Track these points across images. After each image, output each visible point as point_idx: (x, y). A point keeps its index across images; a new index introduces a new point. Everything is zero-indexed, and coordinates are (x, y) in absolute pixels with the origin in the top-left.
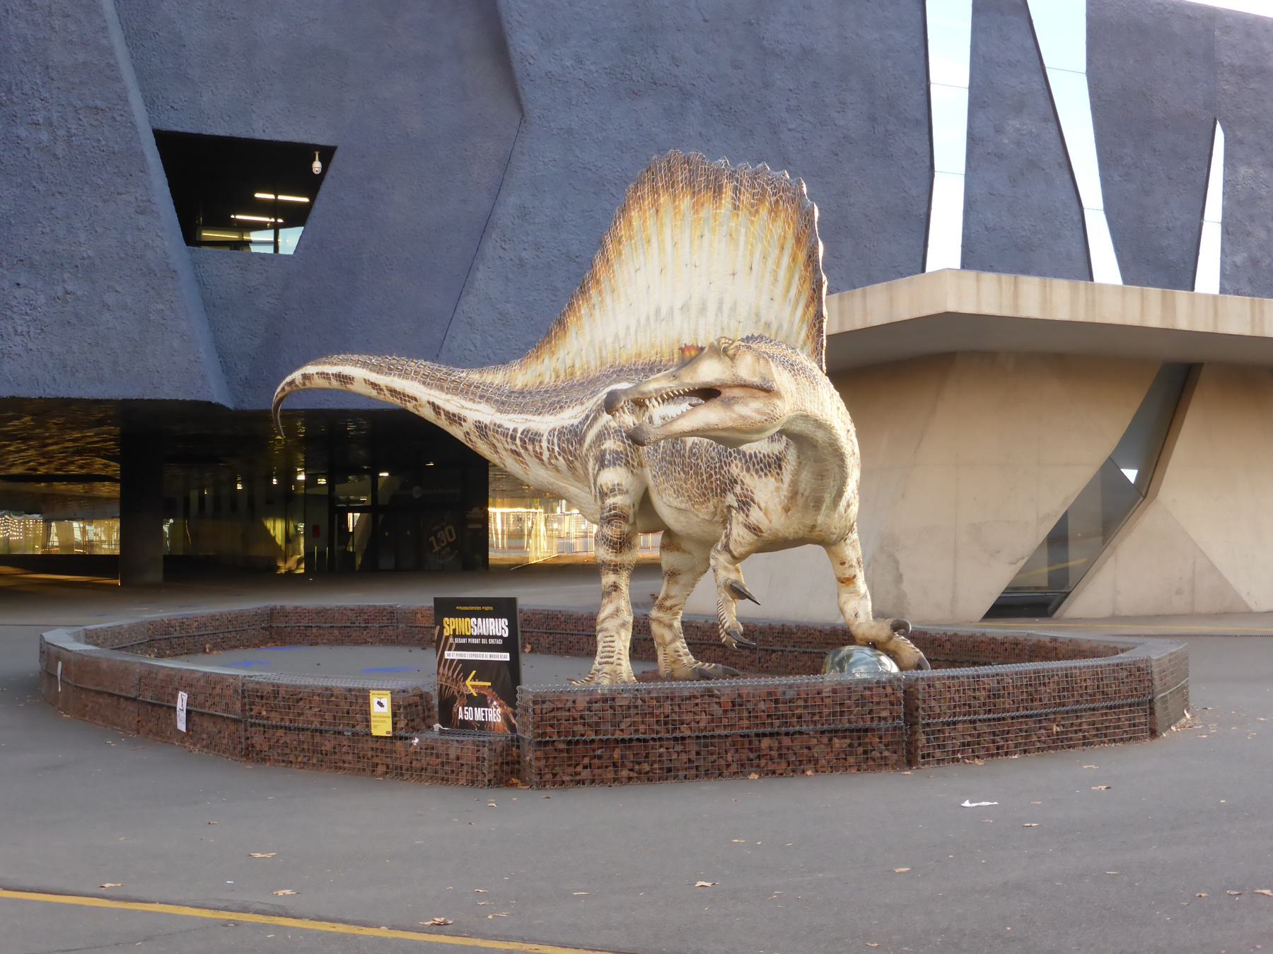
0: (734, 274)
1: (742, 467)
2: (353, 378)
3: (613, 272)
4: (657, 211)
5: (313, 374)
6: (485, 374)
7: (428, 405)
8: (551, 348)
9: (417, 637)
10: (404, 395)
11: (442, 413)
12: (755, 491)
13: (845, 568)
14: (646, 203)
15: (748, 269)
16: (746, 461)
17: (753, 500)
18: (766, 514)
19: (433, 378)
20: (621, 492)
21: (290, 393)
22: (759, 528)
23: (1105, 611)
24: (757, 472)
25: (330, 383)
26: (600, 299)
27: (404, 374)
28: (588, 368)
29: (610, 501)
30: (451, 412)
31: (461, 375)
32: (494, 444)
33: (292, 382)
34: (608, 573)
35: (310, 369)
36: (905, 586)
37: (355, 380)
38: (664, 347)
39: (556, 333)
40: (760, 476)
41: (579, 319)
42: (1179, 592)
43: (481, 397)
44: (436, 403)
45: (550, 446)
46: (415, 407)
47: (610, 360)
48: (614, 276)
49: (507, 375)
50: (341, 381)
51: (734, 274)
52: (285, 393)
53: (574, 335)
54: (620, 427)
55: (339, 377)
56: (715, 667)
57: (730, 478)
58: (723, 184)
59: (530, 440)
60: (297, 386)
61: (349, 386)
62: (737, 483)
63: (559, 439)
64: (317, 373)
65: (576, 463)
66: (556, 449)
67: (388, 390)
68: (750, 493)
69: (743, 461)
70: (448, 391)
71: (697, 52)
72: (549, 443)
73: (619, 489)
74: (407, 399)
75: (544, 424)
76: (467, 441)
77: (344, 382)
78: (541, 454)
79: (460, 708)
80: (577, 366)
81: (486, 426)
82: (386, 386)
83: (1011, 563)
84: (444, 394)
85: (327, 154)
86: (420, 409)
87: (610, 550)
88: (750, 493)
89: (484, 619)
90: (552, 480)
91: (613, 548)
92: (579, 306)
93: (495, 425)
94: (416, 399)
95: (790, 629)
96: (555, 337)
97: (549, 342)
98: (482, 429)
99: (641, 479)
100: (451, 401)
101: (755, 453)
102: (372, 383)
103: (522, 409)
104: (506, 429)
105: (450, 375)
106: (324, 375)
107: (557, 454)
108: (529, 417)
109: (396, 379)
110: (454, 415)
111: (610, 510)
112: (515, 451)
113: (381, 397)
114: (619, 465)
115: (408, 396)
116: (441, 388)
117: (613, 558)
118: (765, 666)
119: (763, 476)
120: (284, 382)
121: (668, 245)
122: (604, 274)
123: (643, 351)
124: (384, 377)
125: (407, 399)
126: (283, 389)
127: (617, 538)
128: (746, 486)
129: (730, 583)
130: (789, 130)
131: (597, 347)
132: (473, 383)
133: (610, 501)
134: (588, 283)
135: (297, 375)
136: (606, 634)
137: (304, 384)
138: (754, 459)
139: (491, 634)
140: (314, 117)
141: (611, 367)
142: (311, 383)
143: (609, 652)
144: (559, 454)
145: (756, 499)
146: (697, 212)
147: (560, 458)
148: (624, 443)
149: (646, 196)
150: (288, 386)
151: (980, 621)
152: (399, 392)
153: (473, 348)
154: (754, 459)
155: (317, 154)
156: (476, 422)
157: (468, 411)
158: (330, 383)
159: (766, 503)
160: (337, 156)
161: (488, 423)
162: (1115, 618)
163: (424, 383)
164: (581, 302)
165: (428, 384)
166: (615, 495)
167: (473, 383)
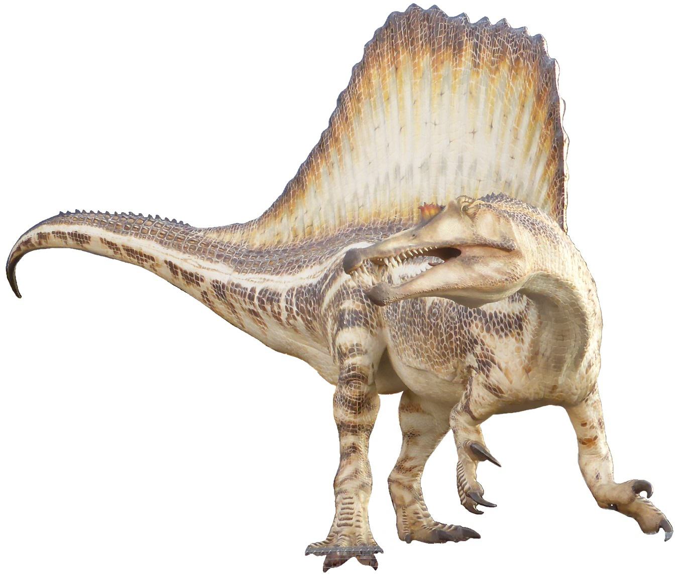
2: (90, 237)
4: (397, 69)
5: (49, 234)
7: (165, 265)
8: (289, 207)
10: (141, 254)
12: (494, 351)
14: (386, 60)
15: (488, 127)
16: (487, 322)
17: (493, 361)
18: (506, 375)
22: (499, 389)
24: (497, 332)
29: (349, 361)
30: (188, 271)
32: (231, 304)
37: (91, 239)
38: (403, 206)
39: (294, 192)
40: (501, 337)
41: (318, 178)
43: (219, 256)
45: (289, 306)
47: (349, 219)
48: (353, 134)
49: (245, 235)
53: (313, 194)
58: (462, 42)
63: (297, 299)
64: (53, 233)
66: (295, 309)
67: (124, 249)
68: (490, 353)
69: (484, 321)
70: (186, 250)
72: (287, 303)
74: (144, 258)
77: (80, 241)
78: (279, 314)
81: (224, 286)
82: (123, 246)
84: (181, 253)
87: (349, 411)
88: (490, 353)
91: (352, 409)
93: (233, 284)
94: (153, 259)
96: (293, 195)
100: (189, 261)
103: (260, 269)
104: (244, 288)
107: (295, 314)
108: (268, 276)
109: (133, 238)
110: (191, 274)
114: (358, 324)
116: (179, 248)
117: (352, 419)
121: (408, 102)
125: (144, 258)
127: (356, 399)
131: (336, 206)
132: (211, 243)
138: (494, 319)
141: (350, 226)
142: (47, 242)
144: (298, 314)
145: (497, 359)
146: (436, 69)
147: (299, 318)
149: (385, 53)
152: (136, 252)
156: (213, 281)
159: (507, 363)
161: (226, 283)
163: (161, 242)
164: (319, 161)
165: (166, 244)
166: (354, 356)
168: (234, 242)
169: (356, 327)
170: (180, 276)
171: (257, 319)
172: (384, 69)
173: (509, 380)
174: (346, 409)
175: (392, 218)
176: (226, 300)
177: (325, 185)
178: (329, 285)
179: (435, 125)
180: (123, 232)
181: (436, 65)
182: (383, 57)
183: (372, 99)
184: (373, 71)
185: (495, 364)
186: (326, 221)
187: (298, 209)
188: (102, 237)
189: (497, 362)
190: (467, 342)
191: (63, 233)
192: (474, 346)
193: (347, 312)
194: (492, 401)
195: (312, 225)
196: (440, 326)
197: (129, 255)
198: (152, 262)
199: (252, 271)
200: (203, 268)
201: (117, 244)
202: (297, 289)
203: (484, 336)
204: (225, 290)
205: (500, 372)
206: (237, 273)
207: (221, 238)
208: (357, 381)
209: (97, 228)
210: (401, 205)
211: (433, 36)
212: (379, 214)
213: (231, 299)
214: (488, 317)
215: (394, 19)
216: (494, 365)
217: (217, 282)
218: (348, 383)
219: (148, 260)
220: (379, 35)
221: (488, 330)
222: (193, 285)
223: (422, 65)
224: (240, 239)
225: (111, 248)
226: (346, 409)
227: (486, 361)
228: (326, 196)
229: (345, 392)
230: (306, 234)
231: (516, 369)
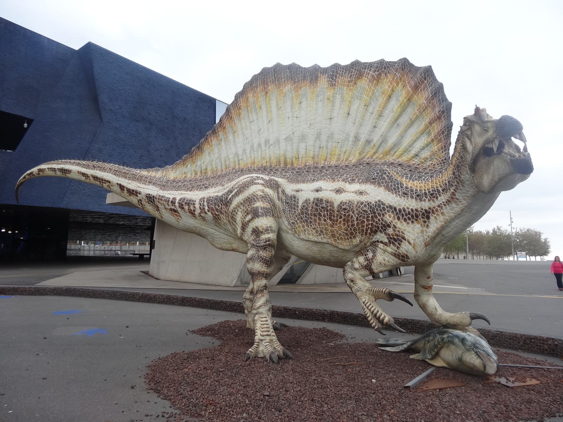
0: (331, 119)
1: (394, 217)
2: (71, 171)
3: (235, 123)
4: (267, 93)
5: (45, 169)
6: (151, 172)
7: (117, 185)
8: (192, 160)
9: (72, 293)
10: (102, 180)
11: (125, 189)
12: (405, 232)
13: (430, 280)
14: (259, 89)
15: (346, 115)
16: (397, 214)
17: (404, 238)
18: (413, 247)
19: (120, 172)
20: (272, 231)
21: (25, 181)
22: (407, 256)
23: (312, 282)
24: (405, 220)
25: (56, 173)
26: (225, 136)
27: (104, 170)
28: (216, 170)
29: (264, 237)
30: (131, 189)
31: (137, 172)
32: (157, 206)
33: (32, 173)
34: (262, 279)
35: (43, 166)
37: (72, 172)
38: (272, 158)
39: (196, 153)
40: (408, 223)
41: (211, 146)
42: (333, 276)
43: (150, 182)
44: (122, 184)
45: (202, 207)
46: (109, 186)
47: (232, 165)
48: (235, 125)
49: (164, 173)
50: (62, 172)
51: (331, 119)
52: (26, 179)
53: (207, 154)
54: (265, 195)
55: (62, 170)
57: (384, 223)
58: (318, 76)
59: (186, 203)
60: (34, 175)
61: (68, 175)
62: (390, 227)
63: (208, 203)
64: (48, 168)
65: (221, 216)
66: (206, 208)
67: (92, 177)
68: (401, 233)
69: (395, 213)
70: (129, 178)
71: (156, 113)
72: (200, 205)
73: (271, 230)
74: (104, 182)
75: (196, 196)
76: (139, 204)
77: (65, 173)
78: (194, 211)
80: (209, 169)
81: (153, 197)
82: (92, 175)
84: (127, 180)
85: (30, 122)
86: (111, 187)
87: (264, 265)
88: (401, 233)
90: (198, 225)
91: (266, 264)
92: (211, 140)
93: (160, 196)
94: (109, 182)
95: (518, 336)
96: (195, 155)
97: (192, 157)
98: (151, 199)
99: (279, 224)
100: (131, 184)
101: (404, 208)
102: (83, 173)
103: (178, 188)
104: (168, 198)
105: (130, 171)
106: (54, 170)
107: (206, 211)
108: (183, 192)
109: (98, 171)
110: (133, 191)
111: (266, 242)
112: (174, 209)
113: (88, 181)
114: (269, 215)
115: (105, 180)
116: (126, 177)
117: (266, 270)
119: (410, 223)
120: (27, 173)
121: (274, 109)
122: (228, 125)
123: (256, 161)
124: (90, 170)
125: (104, 182)
126: (25, 177)
127: (269, 258)
128: (398, 229)
130: (179, 139)
131: (223, 160)
132: (144, 176)
133: (264, 237)
134: (218, 129)
135: (35, 170)
136: (261, 316)
137: (39, 174)
138: (403, 212)
140: (26, 108)
141: (233, 169)
142: (43, 173)
144: (209, 211)
145: (406, 237)
146: (297, 91)
147: (209, 213)
148: (270, 204)
149: (258, 86)
150: (28, 175)
151: (277, 285)
152: (100, 179)
153: (79, 190)
154: (403, 212)
155: (26, 121)
156: (147, 194)
157: (142, 189)
158: (56, 173)
159: (414, 240)
160: (34, 123)
161: (155, 195)
162: (315, 284)
163: (115, 174)
164: (212, 138)
165: (118, 175)
166: (269, 233)
167: (144, 176)
168: (157, 176)
169: (268, 217)
170: (125, 191)
171: (175, 214)
172: (258, 93)
173: (415, 251)
174: (262, 264)
175: (265, 165)
176: (155, 204)
177: (216, 150)
178: (237, 194)
179: (297, 117)
180: (92, 169)
181: (297, 89)
182: (257, 88)
183: (249, 108)
184: (250, 95)
185: (406, 240)
186: (216, 167)
187: (197, 161)
188: (78, 170)
189: (407, 239)
190: (380, 226)
191: (54, 169)
192: (386, 228)
193: (260, 208)
194: (395, 264)
195: (206, 169)
196: (352, 217)
197: (94, 180)
198: (108, 184)
199: (172, 190)
200: (140, 188)
201: (88, 174)
202: (207, 198)
203: (395, 223)
204: (155, 199)
205: (410, 245)
206: (162, 191)
207: (150, 174)
208: (271, 248)
209: (76, 167)
210: (270, 159)
211: (294, 76)
212: (254, 163)
213: (158, 204)
214: (398, 211)
215: (265, 72)
216: (404, 241)
217: (149, 195)
218: (264, 249)
219: (106, 183)
220: (255, 78)
221: (399, 219)
222: (133, 196)
223: (284, 91)
224: (161, 175)
225: (84, 176)
226: (262, 264)
227: (397, 238)
228: (216, 155)
229: (262, 254)
230: (203, 173)
231: (421, 244)
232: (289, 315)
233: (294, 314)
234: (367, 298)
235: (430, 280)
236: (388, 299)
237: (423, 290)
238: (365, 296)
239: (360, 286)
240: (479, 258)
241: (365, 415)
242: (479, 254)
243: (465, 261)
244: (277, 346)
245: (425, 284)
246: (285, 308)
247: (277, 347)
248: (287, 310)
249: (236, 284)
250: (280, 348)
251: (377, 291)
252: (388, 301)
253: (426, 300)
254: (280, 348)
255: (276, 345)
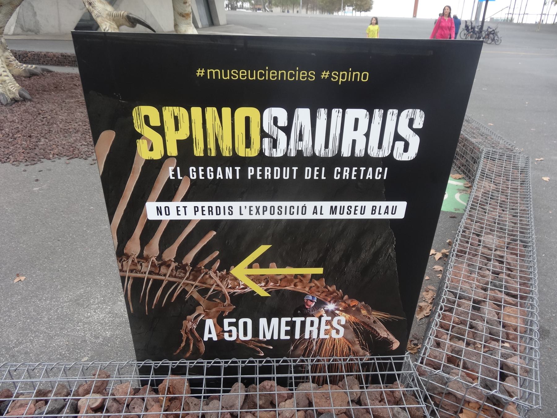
36: (38, 18)
56: (36, 68)
79: (210, 323)
83: (81, 9)
89: (322, 113)
118: (24, 60)
129: (127, 14)
139: (346, 152)
143: (514, 167)
232: (69, 63)
233: (74, 61)
234: (108, 24)
235: (187, 6)
236: (128, 24)
237: (181, 18)
238: (106, 23)
239: (99, 10)
240: (312, 12)
241: (85, 145)
242: (313, 9)
243: (298, 15)
244: (12, 88)
245: (182, 11)
246: (62, 55)
247: (11, 89)
248: (66, 56)
249: (16, 32)
250: (15, 89)
251: (116, 15)
252: (128, 26)
253: (184, 30)
254: (15, 89)
255: (11, 86)
